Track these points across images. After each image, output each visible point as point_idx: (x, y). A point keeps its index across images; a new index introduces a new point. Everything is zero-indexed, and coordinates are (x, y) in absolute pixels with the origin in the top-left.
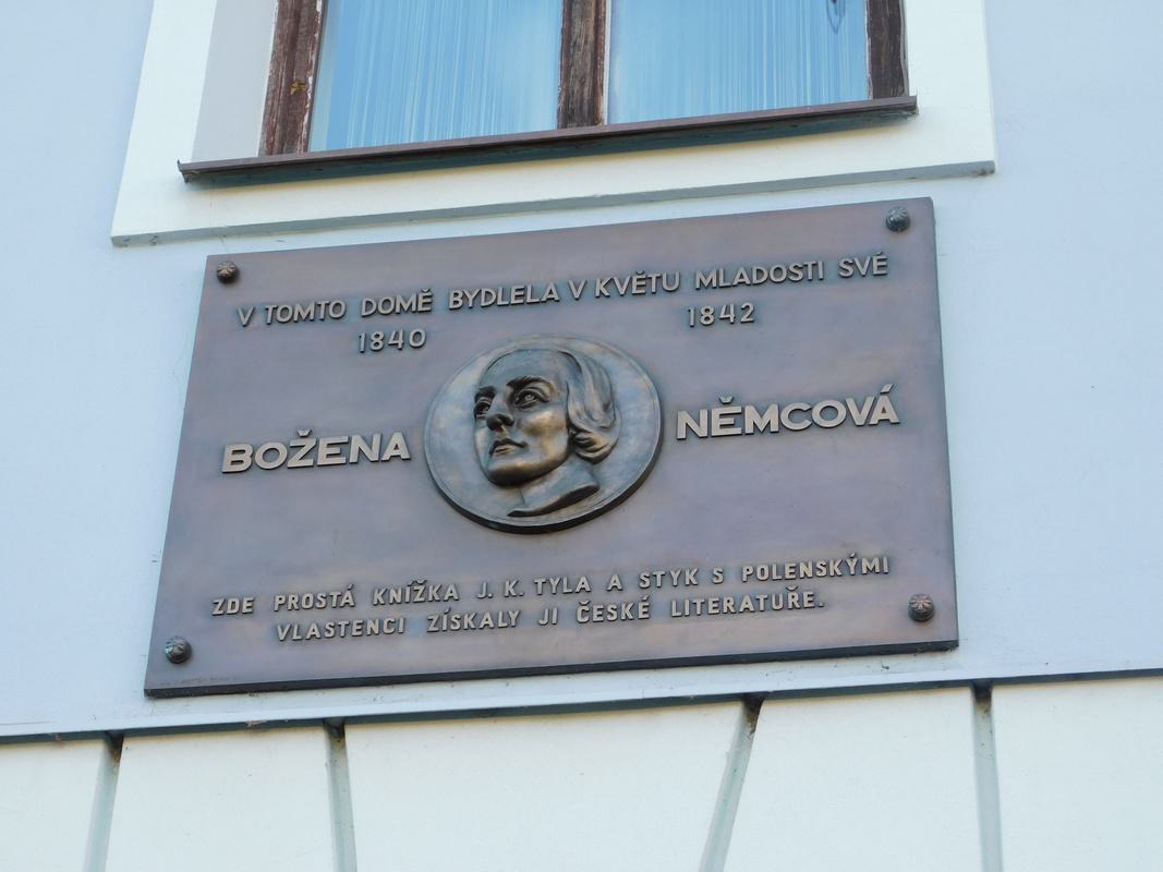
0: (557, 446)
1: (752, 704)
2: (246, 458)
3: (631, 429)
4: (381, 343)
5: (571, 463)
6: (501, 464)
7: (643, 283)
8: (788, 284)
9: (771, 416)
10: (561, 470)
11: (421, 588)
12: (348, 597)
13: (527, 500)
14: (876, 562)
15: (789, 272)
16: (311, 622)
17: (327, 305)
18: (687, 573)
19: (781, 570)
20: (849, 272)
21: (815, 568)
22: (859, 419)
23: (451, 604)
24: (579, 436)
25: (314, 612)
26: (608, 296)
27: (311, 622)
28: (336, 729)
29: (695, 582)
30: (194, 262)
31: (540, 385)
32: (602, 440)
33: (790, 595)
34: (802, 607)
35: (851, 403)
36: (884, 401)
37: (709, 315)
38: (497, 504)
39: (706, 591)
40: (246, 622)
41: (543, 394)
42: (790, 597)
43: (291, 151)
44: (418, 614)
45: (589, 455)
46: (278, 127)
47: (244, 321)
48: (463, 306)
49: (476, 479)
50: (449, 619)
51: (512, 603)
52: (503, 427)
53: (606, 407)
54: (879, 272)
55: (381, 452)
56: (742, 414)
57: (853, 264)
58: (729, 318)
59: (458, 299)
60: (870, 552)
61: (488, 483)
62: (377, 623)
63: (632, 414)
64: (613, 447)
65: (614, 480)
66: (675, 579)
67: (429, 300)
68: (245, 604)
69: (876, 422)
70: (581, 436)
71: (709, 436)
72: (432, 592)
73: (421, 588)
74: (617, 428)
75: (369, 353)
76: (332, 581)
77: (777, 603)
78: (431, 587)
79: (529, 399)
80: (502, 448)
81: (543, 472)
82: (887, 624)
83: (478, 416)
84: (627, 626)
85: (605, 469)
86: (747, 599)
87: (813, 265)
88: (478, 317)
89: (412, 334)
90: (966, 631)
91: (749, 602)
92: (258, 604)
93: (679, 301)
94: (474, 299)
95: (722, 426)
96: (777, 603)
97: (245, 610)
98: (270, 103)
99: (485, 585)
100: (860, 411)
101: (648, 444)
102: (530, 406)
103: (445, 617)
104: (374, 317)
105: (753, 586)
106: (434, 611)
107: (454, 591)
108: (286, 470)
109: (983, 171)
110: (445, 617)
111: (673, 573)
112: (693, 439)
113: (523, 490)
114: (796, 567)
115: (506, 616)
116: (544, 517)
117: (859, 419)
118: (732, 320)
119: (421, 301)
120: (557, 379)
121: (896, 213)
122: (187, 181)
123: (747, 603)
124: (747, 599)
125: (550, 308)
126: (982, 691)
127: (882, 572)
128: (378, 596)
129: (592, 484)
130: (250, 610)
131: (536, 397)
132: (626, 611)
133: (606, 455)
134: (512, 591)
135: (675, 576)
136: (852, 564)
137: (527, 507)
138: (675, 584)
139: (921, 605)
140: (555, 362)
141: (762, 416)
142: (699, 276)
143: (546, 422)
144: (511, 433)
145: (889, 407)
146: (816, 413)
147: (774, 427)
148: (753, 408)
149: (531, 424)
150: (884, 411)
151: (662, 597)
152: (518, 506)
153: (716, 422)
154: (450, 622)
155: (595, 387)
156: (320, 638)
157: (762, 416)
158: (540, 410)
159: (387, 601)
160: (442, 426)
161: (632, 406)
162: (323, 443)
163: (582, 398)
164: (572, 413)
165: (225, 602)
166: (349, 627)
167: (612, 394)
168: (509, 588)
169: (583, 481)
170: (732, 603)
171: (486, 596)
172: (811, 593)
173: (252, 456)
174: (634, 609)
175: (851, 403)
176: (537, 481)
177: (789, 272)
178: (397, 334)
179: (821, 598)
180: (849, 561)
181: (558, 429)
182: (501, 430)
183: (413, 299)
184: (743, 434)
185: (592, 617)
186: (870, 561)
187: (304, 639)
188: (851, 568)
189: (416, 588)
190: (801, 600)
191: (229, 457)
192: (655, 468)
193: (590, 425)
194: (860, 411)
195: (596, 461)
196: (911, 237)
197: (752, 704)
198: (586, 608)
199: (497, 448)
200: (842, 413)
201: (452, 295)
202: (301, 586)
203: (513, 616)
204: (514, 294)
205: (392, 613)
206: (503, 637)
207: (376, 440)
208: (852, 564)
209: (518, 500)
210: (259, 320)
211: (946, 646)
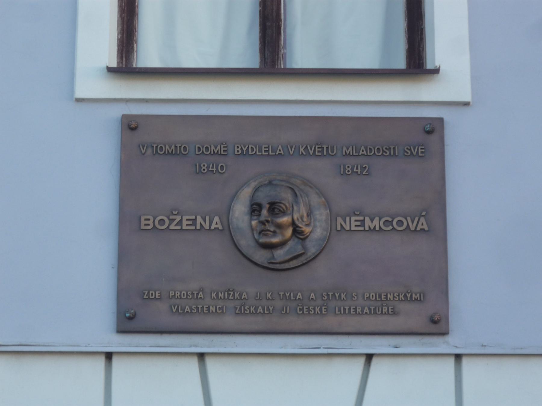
0: (289, 232)
1: (369, 357)
2: (151, 222)
3: (318, 224)
6: (263, 240)
10: (290, 243)
15: (383, 151)
22: (412, 228)
26: (305, 155)
28: (201, 356)
32: (307, 230)
35: (409, 219)
36: (422, 220)
38: (261, 256)
41: (283, 209)
45: (301, 237)
46: (125, 8)
47: (143, 152)
48: (244, 154)
49: (252, 243)
50: (244, 308)
52: (266, 224)
53: (308, 215)
55: (210, 226)
56: (364, 220)
57: (410, 150)
58: (213, 171)
61: (106, 68)
65: (312, 250)
67: (423, 151)
70: (297, 229)
72: (237, 295)
74: (312, 224)
77: (379, 311)
78: (236, 293)
80: (266, 233)
81: (282, 244)
83: (253, 214)
85: (308, 243)
87: (393, 148)
96: (379, 311)
97: (157, 297)
99: (258, 294)
100: (413, 223)
109: (467, 104)
113: (273, 251)
115: (268, 309)
116: (283, 265)
117: (412, 228)
118: (359, 173)
119: (222, 149)
126: (458, 357)
130: (159, 297)
131: (280, 210)
132: (317, 310)
133: (308, 236)
136: (409, 296)
139: (436, 318)
141: (372, 222)
142: (345, 149)
147: (377, 228)
150: (422, 224)
154: (245, 310)
155: (304, 206)
157: (372, 222)
162: (184, 218)
163: (299, 211)
164: (295, 218)
165: (149, 293)
167: (310, 205)
169: (300, 250)
172: (392, 307)
173: (154, 222)
175: (409, 219)
176: (279, 248)
177: (383, 151)
178: (213, 165)
181: (289, 226)
183: (219, 147)
186: (416, 295)
187: (184, 313)
188: (408, 298)
191: (143, 222)
193: (302, 225)
194: (413, 223)
195: (304, 240)
196: (434, 137)
197: (369, 357)
198: (301, 308)
199: (262, 232)
200: (405, 224)
201: (236, 147)
203: (271, 309)
205: (220, 304)
207: (207, 218)
208: (409, 296)
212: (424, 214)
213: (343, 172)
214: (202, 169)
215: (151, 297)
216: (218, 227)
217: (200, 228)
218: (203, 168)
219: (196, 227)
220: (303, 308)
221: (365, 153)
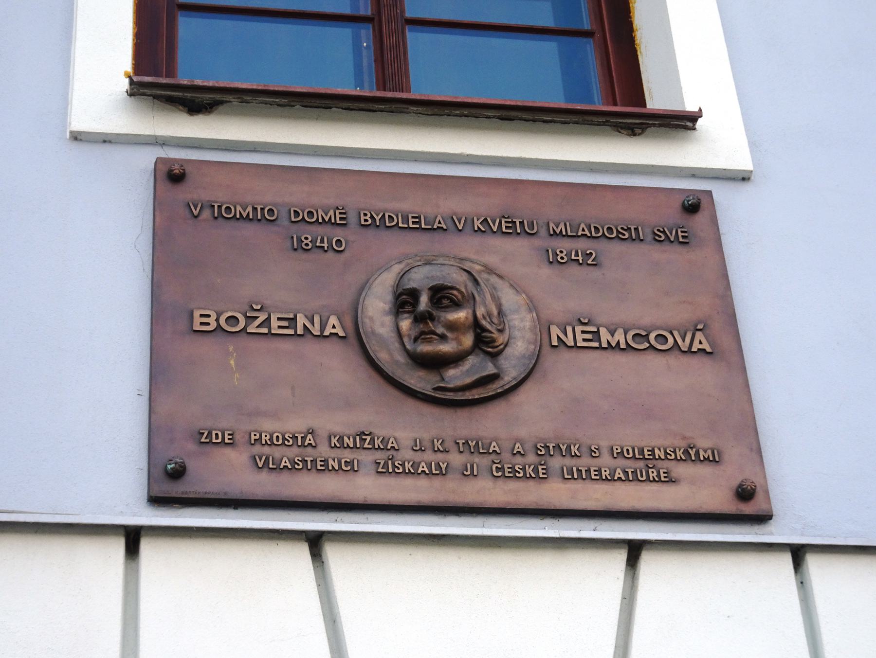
2: (212, 320)
3: (517, 333)
5: (477, 355)
6: (424, 348)
7: (510, 225)
8: (616, 240)
9: (619, 336)
11: (368, 438)
12: (309, 439)
13: (447, 379)
14: (709, 452)
16: (285, 455)
18: (572, 447)
19: (641, 451)
20: (661, 237)
21: (666, 453)
23: (392, 452)
24: (484, 334)
25: (285, 449)
27: (285, 455)
29: (578, 454)
30: (147, 158)
31: (455, 292)
33: (650, 471)
34: (660, 481)
36: (699, 336)
37: (563, 255)
39: (585, 462)
40: (228, 451)
42: (650, 473)
44: (367, 458)
47: (196, 213)
51: (440, 456)
55: (322, 330)
56: (598, 332)
57: (664, 232)
59: (367, 218)
60: (703, 443)
62: (336, 460)
63: (516, 323)
64: (506, 345)
65: (511, 369)
66: (564, 451)
68: (227, 437)
69: (696, 350)
71: (321, 336)
72: (377, 442)
73: (368, 438)
75: (300, 251)
76: (295, 425)
78: (376, 438)
79: (446, 302)
82: (722, 501)
84: (531, 483)
85: (502, 361)
86: (619, 470)
88: (385, 234)
89: (339, 238)
90: (777, 507)
91: (621, 472)
92: (237, 437)
93: (537, 242)
94: (380, 220)
95: (279, 327)
97: (227, 441)
101: (533, 347)
102: (447, 307)
104: (300, 223)
105: (621, 462)
106: (380, 456)
107: (394, 442)
108: (245, 334)
109: (744, 178)
110: (390, 462)
111: (561, 446)
112: (562, 347)
113: (441, 370)
114: (653, 451)
119: (338, 216)
120: (466, 287)
121: (693, 199)
122: (131, 94)
123: (619, 474)
124: (619, 470)
125: (437, 236)
127: (714, 460)
128: (334, 441)
129: (494, 371)
131: (452, 300)
134: (336, 443)
135: (564, 448)
136: (692, 452)
137: (449, 384)
139: (748, 485)
140: (462, 276)
141: (613, 336)
143: (462, 320)
144: (434, 326)
145: (704, 340)
146: (652, 336)
148: (605, 329)
149: (450, 321)
150: (701, 343)
152: (437, 382)
154: (394, 466)
156: (292, 469)
157: (613, 336)
158: (456, 310)
159: (343, 446)
160: (370, 314)
161: (516, 317)
164: (479, 313)
166: (314, 462)
168: (437, 444)
169: (490, 369)
170: (608, 472)
171: (420, 449)
173: (217, 320)
174: (536, 470)
175: (676, 333)
179: (674, 475)
180: (690, 450)
182: (427, 324)
184: (601, 348)
185: (503, 474)
186: (705, 451)
187: (278, 469)
189: (364, 437)
190: (659, 475)
191: (197, 320)
192: (536, 368)
196: (700, 219)
200: (671, 341)
201: (362, 215)
202: (268, 425)
203: (443, 466)
204: (411, 220)
205: (347, 455)
206: (437, 482)
209: (438, 378)
210: (206, 214)
211: (763, 518)
214: (303, 244)
218: (306, 242)
219: (296, 331)
221: (587, 232)
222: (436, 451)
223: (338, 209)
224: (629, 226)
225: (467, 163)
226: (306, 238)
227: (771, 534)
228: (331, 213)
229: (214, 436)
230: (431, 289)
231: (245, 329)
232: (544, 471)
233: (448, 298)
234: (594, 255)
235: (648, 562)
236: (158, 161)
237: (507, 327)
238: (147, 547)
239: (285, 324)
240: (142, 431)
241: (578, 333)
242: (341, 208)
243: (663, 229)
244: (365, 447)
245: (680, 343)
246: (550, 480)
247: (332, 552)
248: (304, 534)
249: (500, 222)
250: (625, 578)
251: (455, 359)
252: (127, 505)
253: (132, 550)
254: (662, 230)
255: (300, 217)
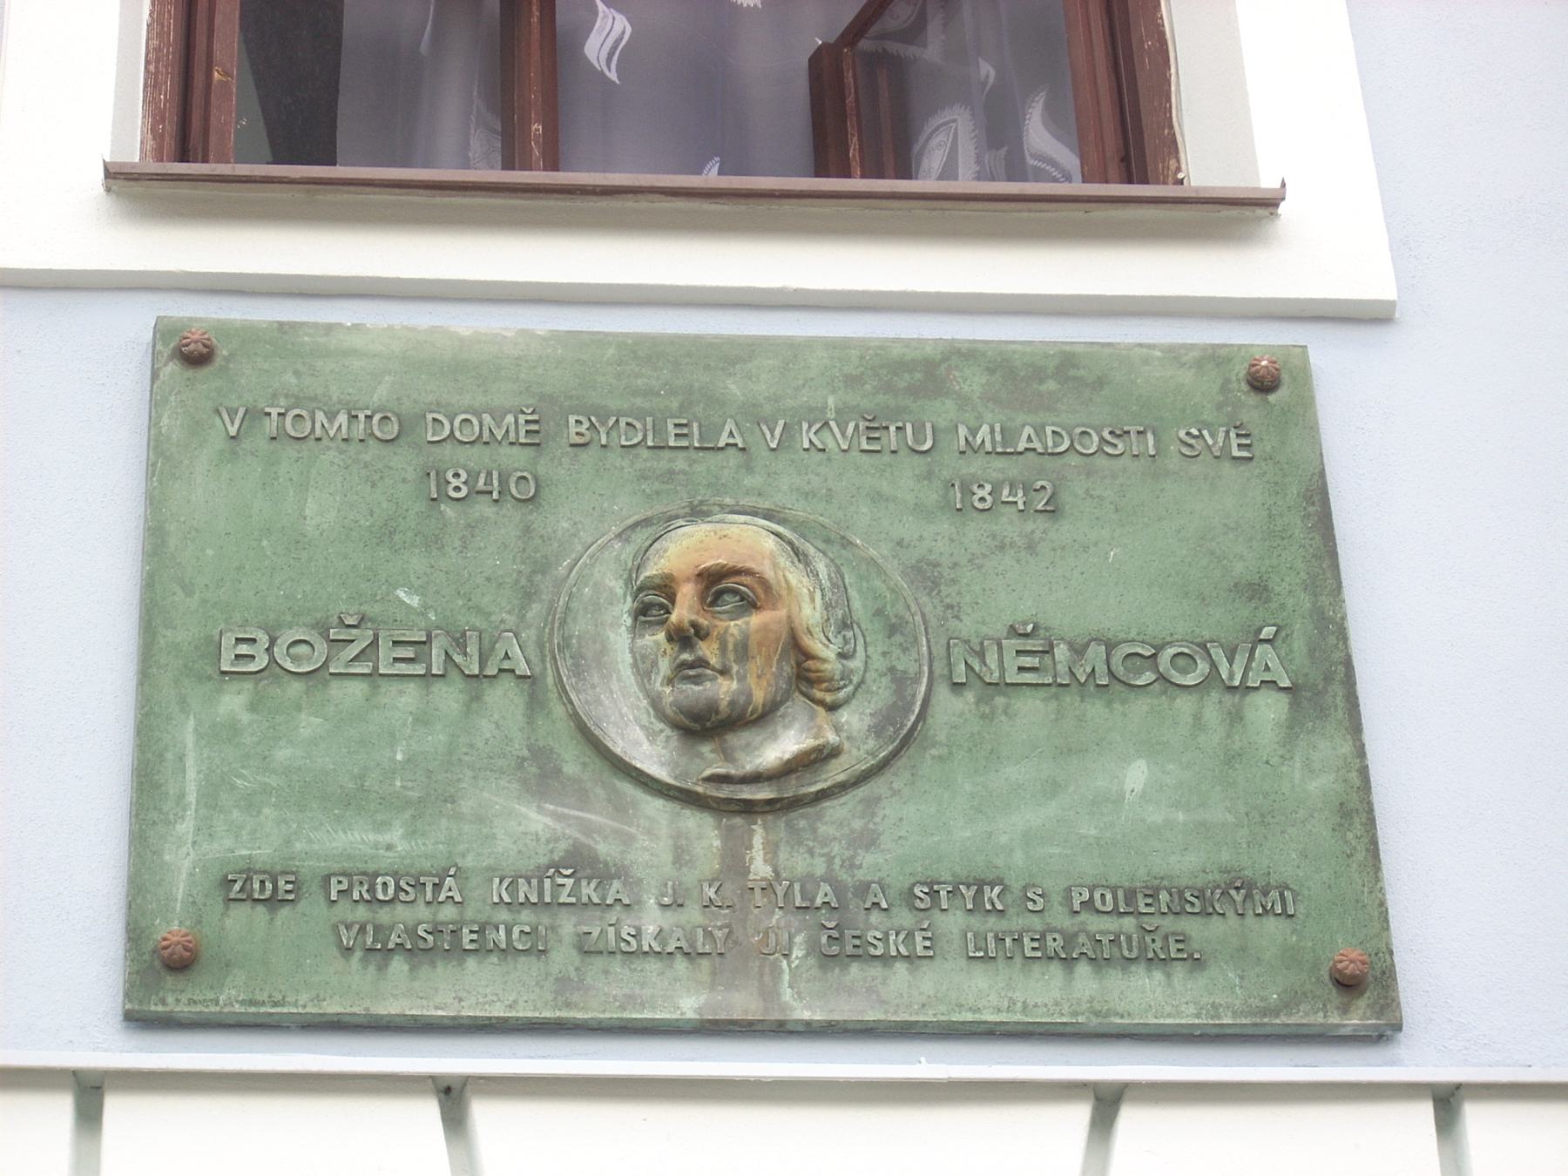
4: (989, 498)
15: (1102, 439)
17: (369, 417)
43: (698, 171)
54: (866, 447)
58: (1016, 503)
59: (583, 429)
67: (534, 427)
70: (810, 664)
98: (152, 68)
103: (612, 929)
138: (970, 906)
151: (952, 922)
153: (1012, 663)
177: (1102, 439)
198: (835, 934)
212: (1268, 632)
213: (962, 501)
214: (976, 497)
215: (381, 896)
216: (512, 667)
217: (445, 669)
218: (455, 482)
219: (429, 667)
220: (842, 934)
221: (1037, 445)
222: (1259, 915)
223: (523, 413)
224: (1126, 429)
225: (56, 288)
226: (457, 475)
227: (1392, 1063)
228: (510, 419)
229: (379, 888)
230: (701, 575)
231: (325, 665)
232: (928, 943)
233: (735, 592)
234: (1049, 491)
235: (1130, 1119)
236: (164, 330)
237: (860, 648)
238: (116, 1107)
239: (408, 652)
240: (114, 878)
241: (1009, 656)
242: (530, 410)
243: (1199, 431)
244: (561, 901)
245: (977, 668)
246: (938, 961)
247: (483, 1113)
248: (430, 1081)
249: (1227, 433)
250: (450, 1158)
251: (759, 718)
252: (81, 1028)
253: (89, 1115)
254: (1196, 433)
255: (447, 432)
